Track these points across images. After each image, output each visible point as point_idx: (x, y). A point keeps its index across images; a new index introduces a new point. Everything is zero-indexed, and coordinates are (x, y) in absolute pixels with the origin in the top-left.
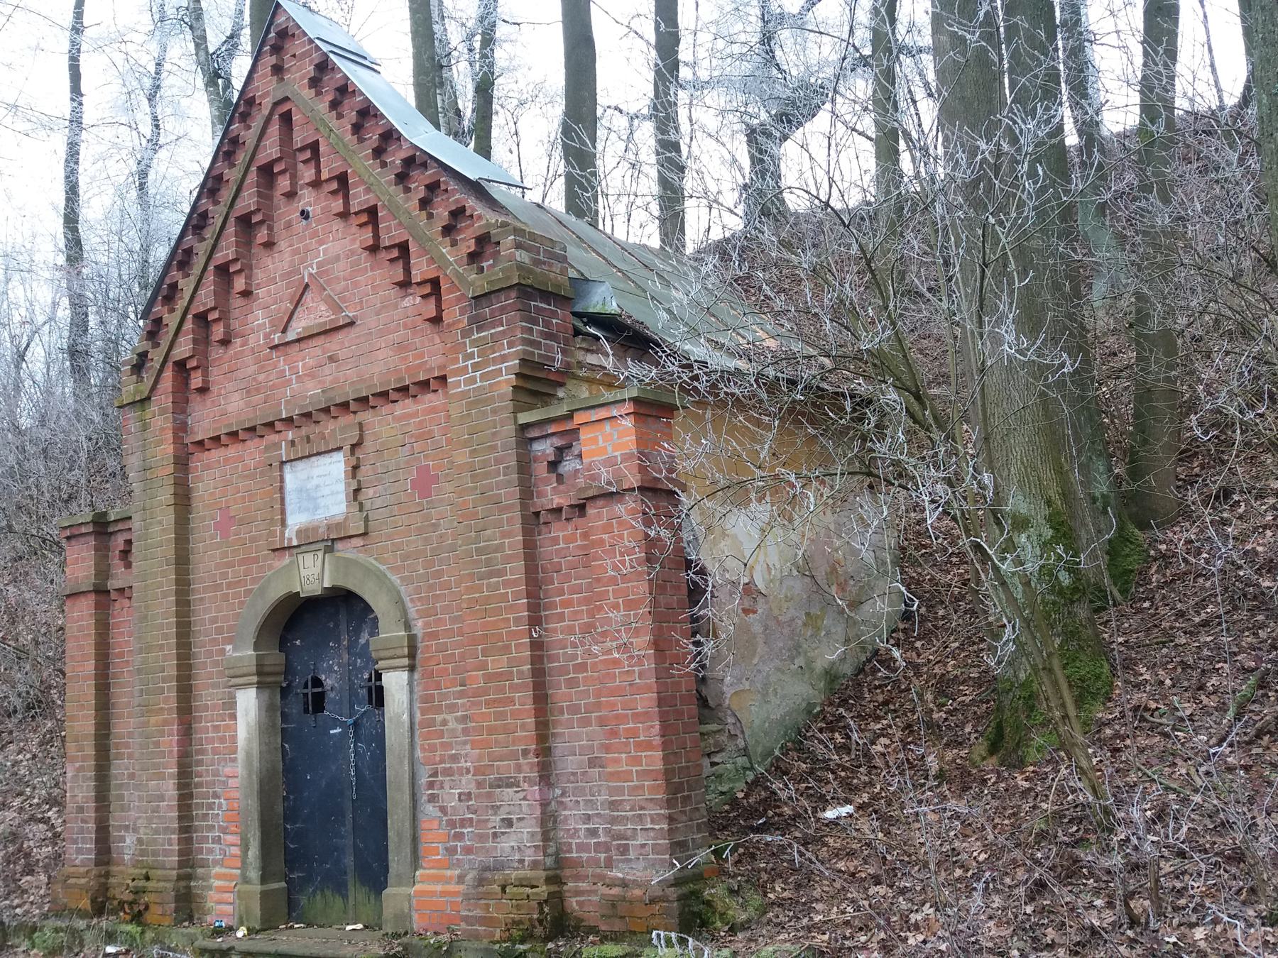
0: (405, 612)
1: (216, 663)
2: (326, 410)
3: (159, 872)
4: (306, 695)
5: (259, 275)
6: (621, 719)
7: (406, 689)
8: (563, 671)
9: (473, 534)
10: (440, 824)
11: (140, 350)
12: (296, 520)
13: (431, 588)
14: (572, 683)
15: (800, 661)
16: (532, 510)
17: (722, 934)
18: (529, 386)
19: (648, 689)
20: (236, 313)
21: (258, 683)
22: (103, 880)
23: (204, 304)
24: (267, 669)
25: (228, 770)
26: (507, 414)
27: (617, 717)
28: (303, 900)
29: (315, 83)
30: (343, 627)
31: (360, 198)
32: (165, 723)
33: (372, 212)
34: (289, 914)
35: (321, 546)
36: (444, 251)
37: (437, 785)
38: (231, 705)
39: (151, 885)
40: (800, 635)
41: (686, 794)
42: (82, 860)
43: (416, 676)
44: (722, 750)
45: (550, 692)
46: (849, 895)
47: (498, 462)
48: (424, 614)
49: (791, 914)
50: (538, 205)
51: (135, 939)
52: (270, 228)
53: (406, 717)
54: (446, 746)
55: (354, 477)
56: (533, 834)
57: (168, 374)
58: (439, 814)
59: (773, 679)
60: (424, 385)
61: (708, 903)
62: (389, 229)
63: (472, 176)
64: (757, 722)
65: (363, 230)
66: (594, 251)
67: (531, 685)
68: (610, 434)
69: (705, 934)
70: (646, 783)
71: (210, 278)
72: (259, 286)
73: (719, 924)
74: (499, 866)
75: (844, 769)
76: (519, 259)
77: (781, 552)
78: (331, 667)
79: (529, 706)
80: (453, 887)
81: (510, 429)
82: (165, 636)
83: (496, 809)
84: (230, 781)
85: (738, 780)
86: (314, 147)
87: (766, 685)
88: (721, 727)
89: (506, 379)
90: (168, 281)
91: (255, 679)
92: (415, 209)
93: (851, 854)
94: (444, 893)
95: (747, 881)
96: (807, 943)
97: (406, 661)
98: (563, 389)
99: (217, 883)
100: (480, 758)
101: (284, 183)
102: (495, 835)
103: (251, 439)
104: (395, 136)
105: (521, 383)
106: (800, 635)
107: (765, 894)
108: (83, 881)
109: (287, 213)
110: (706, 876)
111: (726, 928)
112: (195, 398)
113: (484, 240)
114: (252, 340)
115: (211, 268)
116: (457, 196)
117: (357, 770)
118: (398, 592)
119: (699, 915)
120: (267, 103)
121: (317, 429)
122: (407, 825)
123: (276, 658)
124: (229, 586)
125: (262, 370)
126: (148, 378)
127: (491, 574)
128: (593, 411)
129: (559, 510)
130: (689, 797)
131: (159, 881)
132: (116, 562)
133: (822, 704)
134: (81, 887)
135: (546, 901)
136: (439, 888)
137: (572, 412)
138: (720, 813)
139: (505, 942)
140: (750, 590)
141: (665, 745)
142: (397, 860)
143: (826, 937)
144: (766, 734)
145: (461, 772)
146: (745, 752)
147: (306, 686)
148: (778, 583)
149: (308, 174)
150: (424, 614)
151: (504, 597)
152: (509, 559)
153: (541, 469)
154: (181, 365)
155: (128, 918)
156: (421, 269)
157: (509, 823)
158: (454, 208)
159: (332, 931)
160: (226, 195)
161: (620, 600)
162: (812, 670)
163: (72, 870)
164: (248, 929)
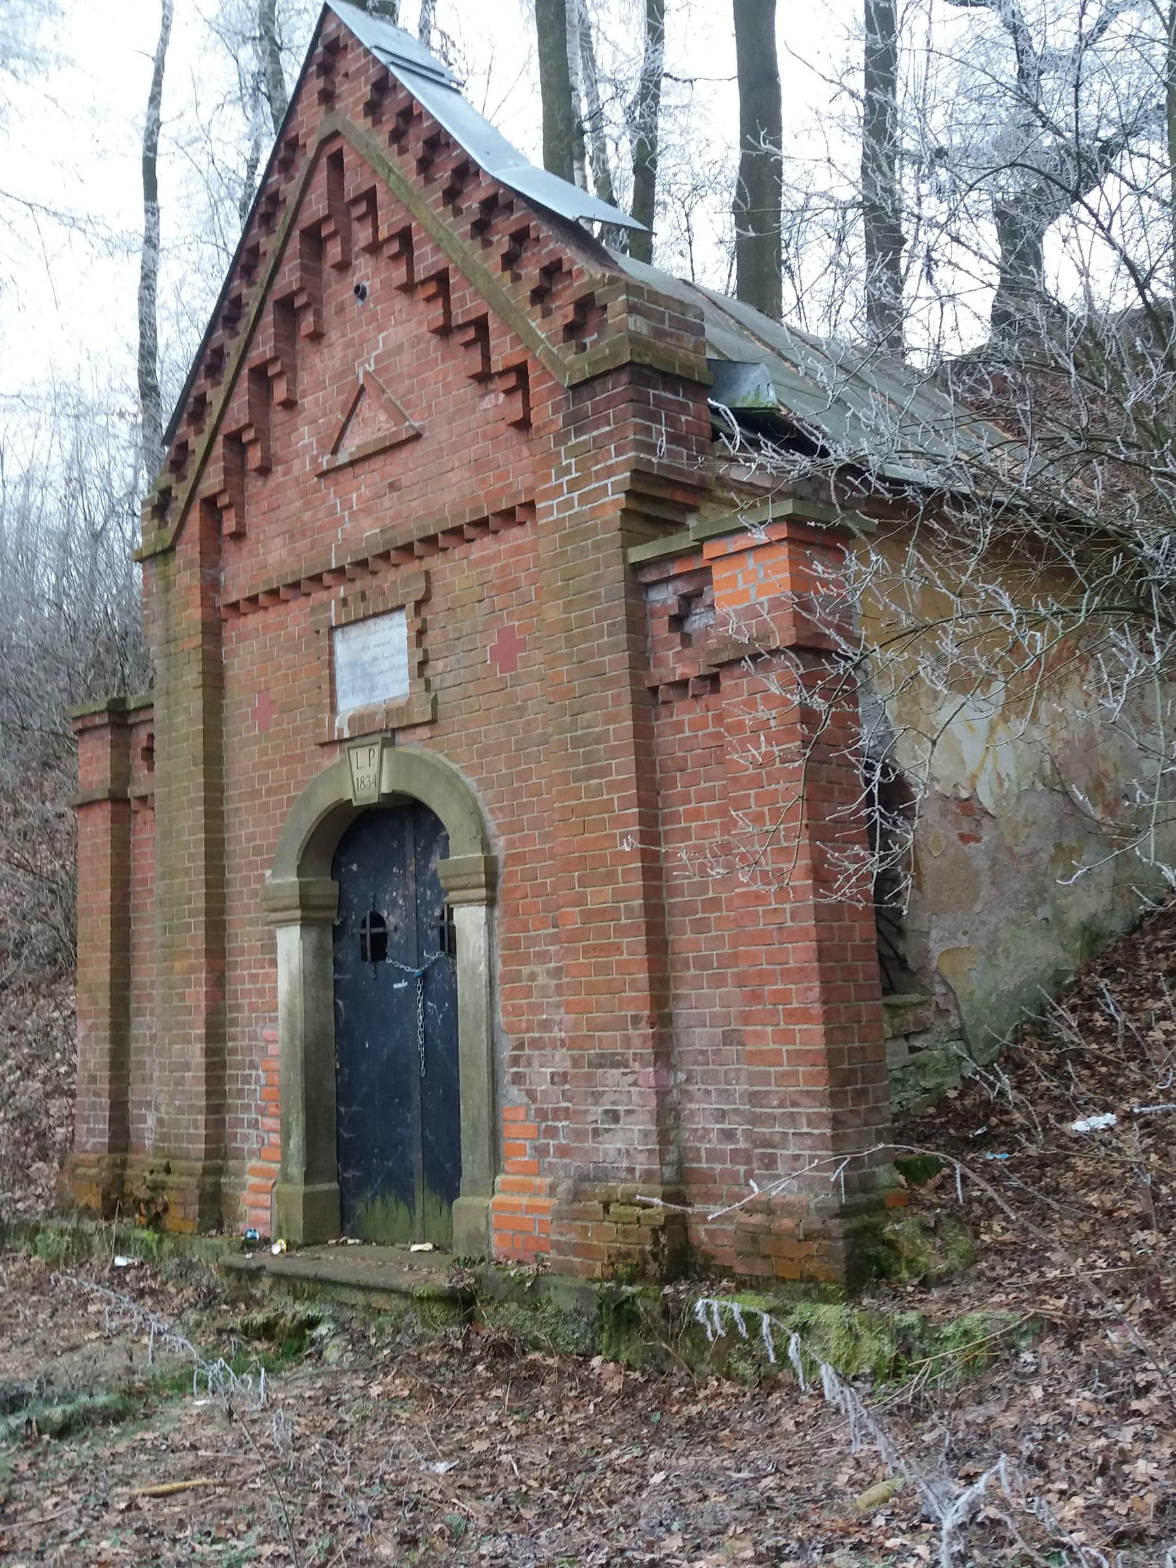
0: (482, 826)
1: (254, 894)
2: (385, 556)
3: (182, 1164)
4: (363, 937)
5: (305, 379)
6: (765, 977)
7: (483, 929)
8: (689, 908)
9: (567, 718)
10: (527, 1114)
11: (163, 485)
12: (349, 704)
13: (516, 793)
14: (701, 926)
15: (1045, 911)
16: (647, 684)
17: (910, 1289)
18: (645, 509)
19: (803, 934)
20: (277, 432)
21: (302, 919)
22: (118, 1171)
23: (237, 421)
24: (314, 901)
25: (267, 1033)
26: (614, 550)
27: (760, 973)
28: (360, 1209)
29: (372, 109)
30: (409, 846)
31: (426, 261)
32: (192, 969)
33: (441, 278)
34: (342, 1225)
35: (378, 738)
36: (533, 324)
37: (523, 1062)
38: (270, 947)
39: (172, 1180)
40: (1045, 874)
41: (859, 1086)
42: (94, 1145)
43: (497, 913)
44: (925, 1031)
45: (671, 937)
46: (1102, 1242)
47: (600, 617)
48: (510, 828)
49: (1014, 1265)
50: (685, 282)
51: (151, 1251)
52: (318, 314)
53: (483, 968)
54: (535, 1008)
55: (419, 644)
56: (646, 1134)
57: (195, 516)
58: (526, 1100)
59: (1003, 934)
60: (508, 516)
61: (891, 1244)
62: (462, 299)
63: (569, 215)
64: (979, 994)
65: (432, 306)
66: (759, 339)
67: (644, 926)
68: (755, 571)
69: (884, 1288)
70: (801, 1069)
71: (244, 384)
72: (304, 394)
73: (905, 1274)
74: (602, 1176)
75: (1106, 1062)
76: (632, 327)
77: (1019, 757)
78: (394, 900)
79: (641, 956)
80: (542, 1201)
81: (617, 571)
82: (192, 858)
83: (597, 1096)
84: (270, 1047)
85: (950, 1073)
86: (370, 196)
87: (993, 943)
88: (925, 998)
89: (613, 500)
90: (194, 392)
91: (298, 913)
92: (496, 270)
93: (1107, 1184)
94: (530, 1209)
95: (949, 1216)
96: (1032, 1311)
97: (482, 892)
98: (695, 515)
99: (251, 1180)
100: (577, 1025)
101: (334, 251)
102: (596, 1132)
103: (296, 598)
104: (472, 170)
105: (633, 505)
106: (1045, 874)
107: (977, 1235)
108: (93, 1171)
109: (339, 291)
110: (888, 1204)
111: (916, 1281)
112: (229, 547)
113: (587, 306)
114: (296, 465)
115: (245, 372)
116: (551, 246)
117: (425, 1039)
118: (474, 801)
119: (876, 1260)
120: (312, 143)
121: (376, 582)
122: (485, 1113)
123: (326, 887)
124: (270, 792)
125: (308, 505)
126: (172, 522)
127: (590, 774)
128: (730, 540)
129: (683, 684)
130: (864, 1092)
131: (181, 1174)
132: (138, 762)
133: (1077, 973)
134: (90, 1179)
135: (663, 1228)
136: (524, 1200)
137: (702, 540)
138: (922, 1117)
139: (608, 1281)
140: (969, 808)
141: (828, 1017)
142: (472, 1160)
143: (1061, 1303)
144: (992, 1010)
145: (554, 1044)
146: (960, 1034)
147: (364, 926)
148: (1013, 800)
149: (363, 235)
150: (510, 828)
151: (608, 806)
152: (613, 752)
153: (660, 627)
154: (210, 503)
155: (144, 1221)
156: (503, 353)
157: (614, 1116)
158: (547, 263)
159: (393, 1251)
160: (263, 272)
161: (766, 809)
162: (1062, 924)
163: (83, 1156)
164: (288, 1243)
